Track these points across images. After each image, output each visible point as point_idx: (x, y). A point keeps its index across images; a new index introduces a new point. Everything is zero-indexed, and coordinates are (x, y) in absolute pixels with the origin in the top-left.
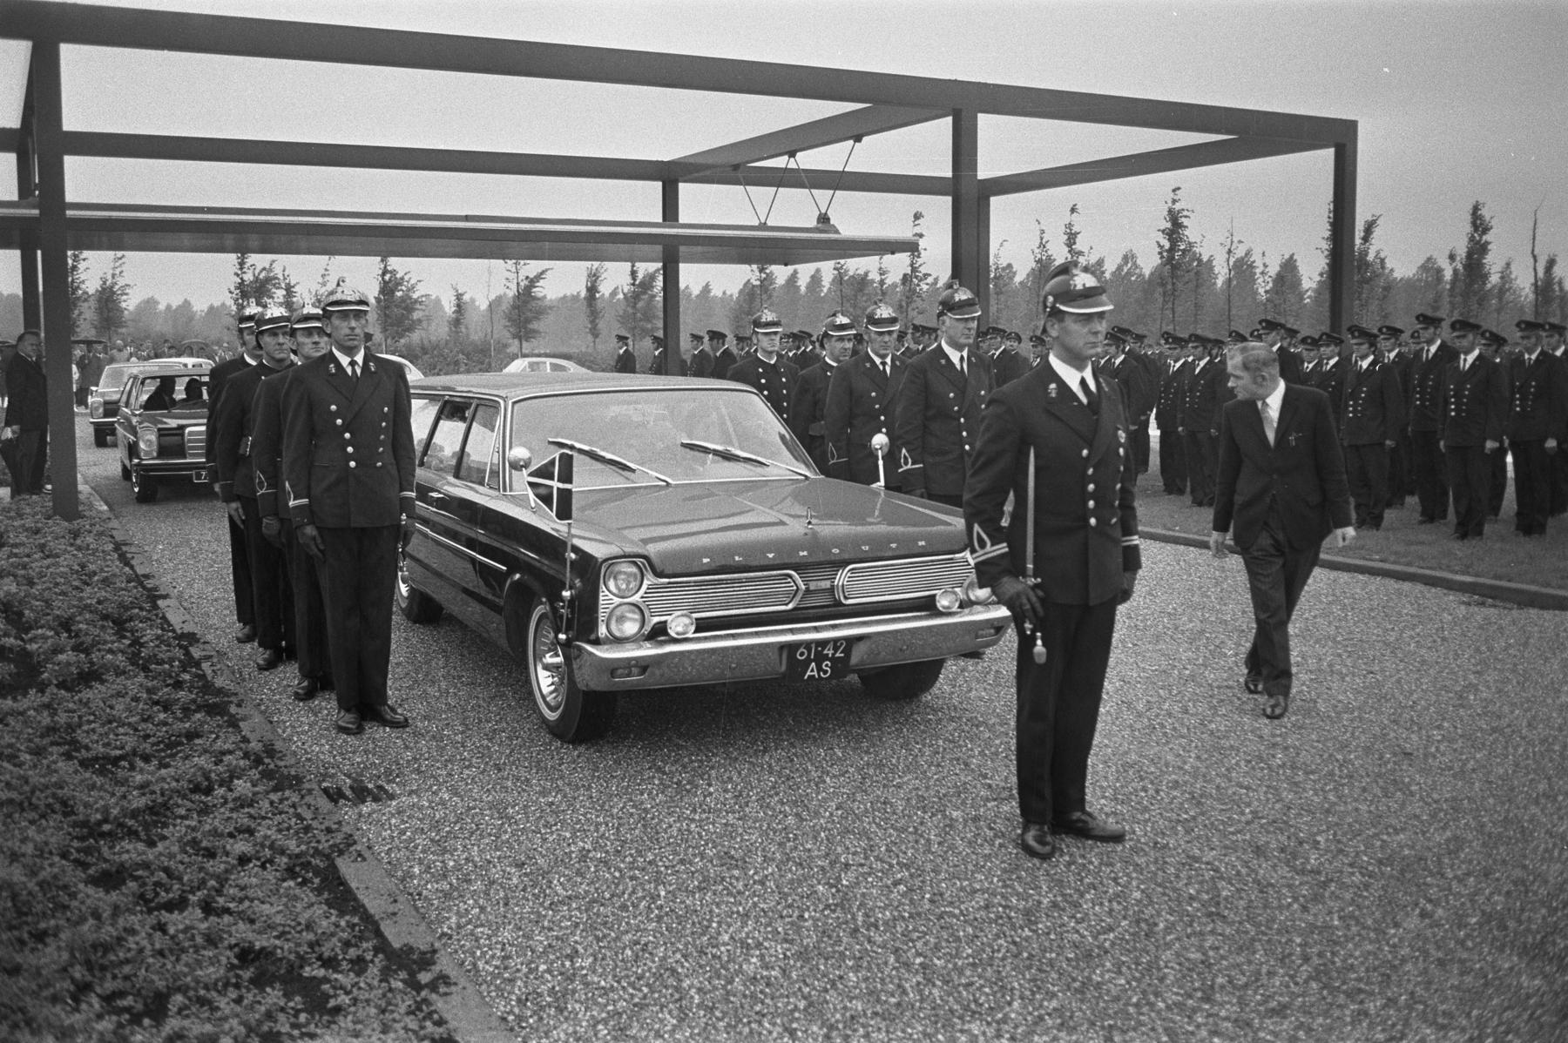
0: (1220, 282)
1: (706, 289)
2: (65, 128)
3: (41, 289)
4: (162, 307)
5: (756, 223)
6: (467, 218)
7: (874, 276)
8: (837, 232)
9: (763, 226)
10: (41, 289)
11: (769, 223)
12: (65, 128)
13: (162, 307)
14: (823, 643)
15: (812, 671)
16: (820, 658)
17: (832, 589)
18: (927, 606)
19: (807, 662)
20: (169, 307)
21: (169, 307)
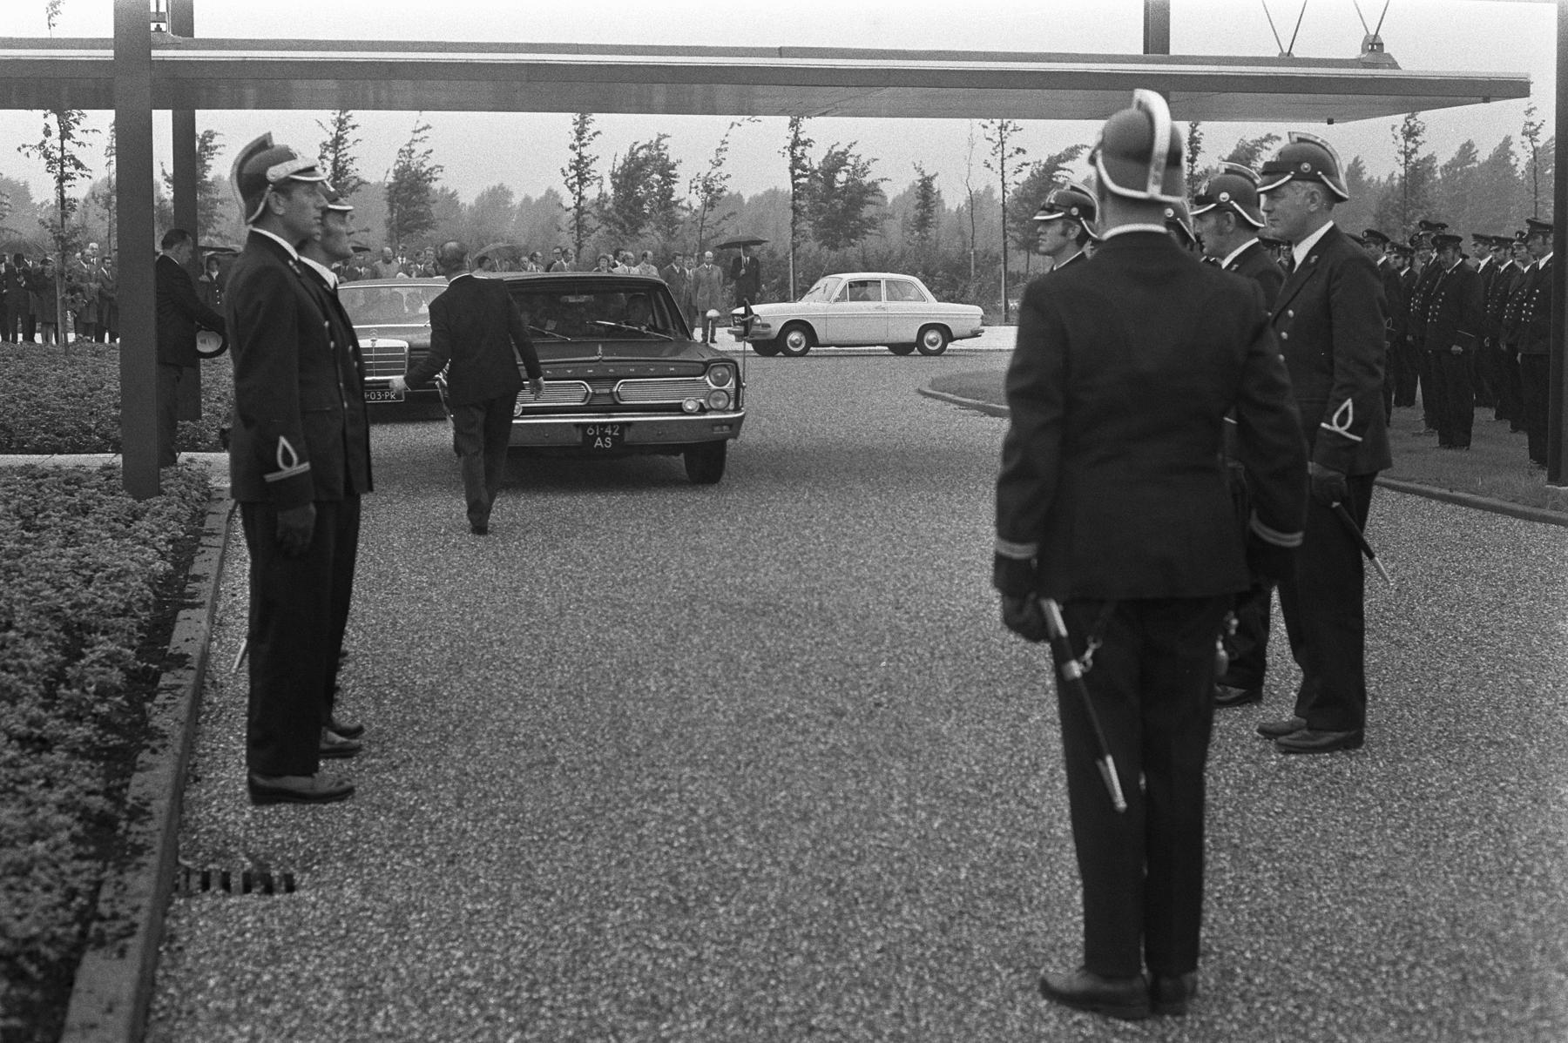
0: (1521, 167)
1: (926, 192)
2: (170, 112)
3: (1419, 388)
4: (516, 200)
5: (1274, 52)
6: (781, 52)
7: (896, 185)
8: (1395, 65)
9: (1287, 59)
10: (1419, 388)
11: (1297, 53)
12: (170, 112)
13: (516, 200)
14: (604, 425)
15: (598, 443)
16: (603, 436)
17: (611, 394)
18: (678, 409)
19: (595, 437)
20: (527, 199)
21: (527, 199)
